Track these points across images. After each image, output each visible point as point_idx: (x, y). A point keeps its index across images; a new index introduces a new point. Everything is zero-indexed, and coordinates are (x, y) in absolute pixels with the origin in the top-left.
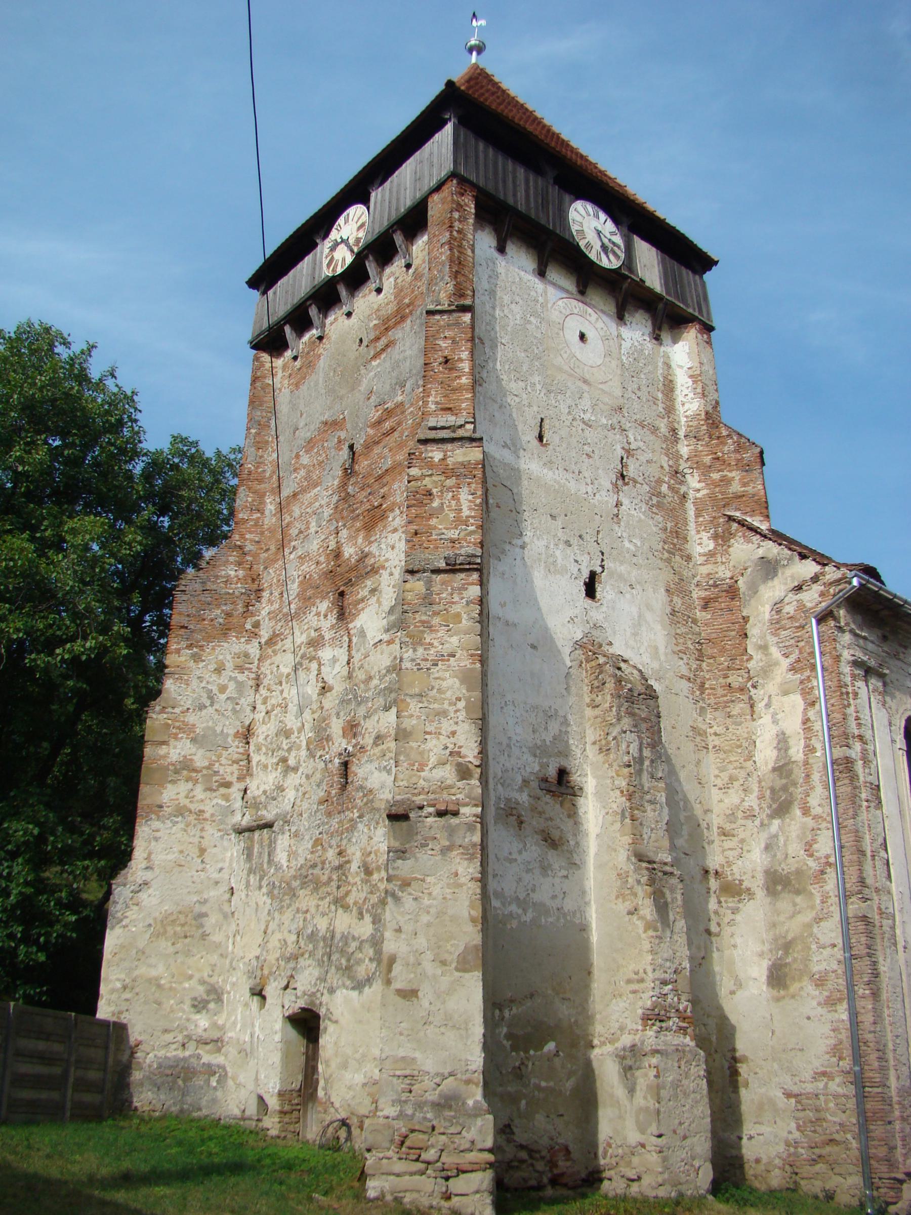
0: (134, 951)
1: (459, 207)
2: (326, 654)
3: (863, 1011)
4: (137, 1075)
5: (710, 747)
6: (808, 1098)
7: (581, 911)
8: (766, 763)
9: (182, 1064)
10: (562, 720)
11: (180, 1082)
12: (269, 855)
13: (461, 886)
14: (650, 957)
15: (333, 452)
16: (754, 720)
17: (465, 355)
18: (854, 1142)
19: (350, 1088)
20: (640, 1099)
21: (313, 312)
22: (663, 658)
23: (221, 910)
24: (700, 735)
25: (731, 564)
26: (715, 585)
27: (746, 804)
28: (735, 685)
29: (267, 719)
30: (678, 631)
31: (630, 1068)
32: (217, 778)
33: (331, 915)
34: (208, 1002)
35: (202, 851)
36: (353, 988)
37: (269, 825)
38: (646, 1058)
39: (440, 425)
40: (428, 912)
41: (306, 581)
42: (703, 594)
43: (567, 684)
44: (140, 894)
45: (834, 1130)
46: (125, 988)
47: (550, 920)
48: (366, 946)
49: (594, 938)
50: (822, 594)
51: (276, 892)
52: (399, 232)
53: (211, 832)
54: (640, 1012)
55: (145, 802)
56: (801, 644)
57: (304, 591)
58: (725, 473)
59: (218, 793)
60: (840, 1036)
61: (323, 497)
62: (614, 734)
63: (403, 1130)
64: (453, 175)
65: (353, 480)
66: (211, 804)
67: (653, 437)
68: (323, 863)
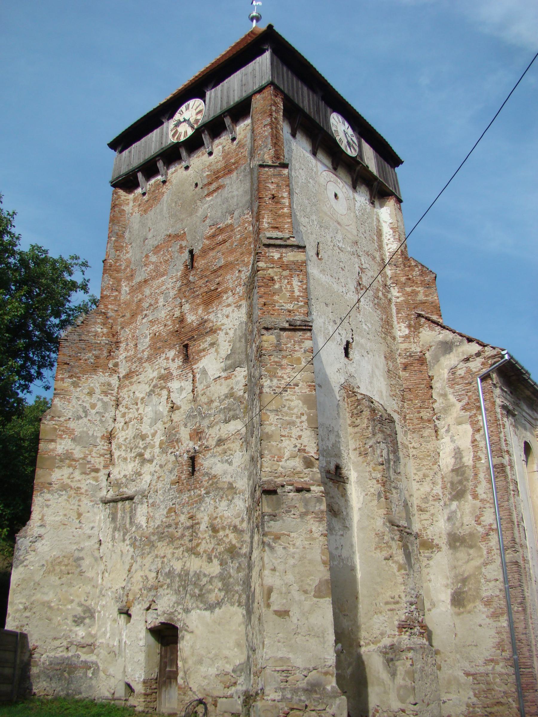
0: (32, 583)
1: (275, 104)
2: (174, 385)
3: (517, 621)
4: (34, 670)
5: (411, 456)
6: (481, 676)
7: (351, 558)
8: (447, 467)
9: (67, 661)
10: (336, 434)
11: (66, 674)
12: (131, 518)
13: (315, 539)
14: (403, 587)
15: (176, 254)
16: (438, 440)
17: (285, 195)
18: (514, 703)
19: (205, 678)
20: (400, 680)
21: (160, 164)
22: (385, 399)
23: (93, 555)
24: (405, 448)
25: (421, 343)
26: (411, 356)
27: (434, 492)
28: (425, 418)
29: (125, 427)
30: (392, 383)
31: (392, 660)
32: (89, 466)
33: (184, 559)
34: (84, 618)
35: (80, 515)
36: (205, 609)
37: (130, 498)
38: (403, 653)
39: (274, 236)
40: (293, 557)
41: (155, 337)
42: (404, 361)
43: (338, 411)
44: (36, 544)
45: (500, 696)
46: (25, 609)
47: (335, 563)
48: (216, 580)
49: (359, 575)
50: (483, 364)
51: (137, 543)
52: (228, 117)
53: (85, 501)
54: (396, 623)
55: (39, 481)
56: (469, 394)
57: (155, 343)
58: (414, 288)
59: (90, 476)
60: (502, 637)
61: (170, 282)
62: (370, 444)
63: (286, 709)
64: (271, 83)
65: (192, 273)
66: (85, 483)
67: (373, 263)
68: (177, 524)
